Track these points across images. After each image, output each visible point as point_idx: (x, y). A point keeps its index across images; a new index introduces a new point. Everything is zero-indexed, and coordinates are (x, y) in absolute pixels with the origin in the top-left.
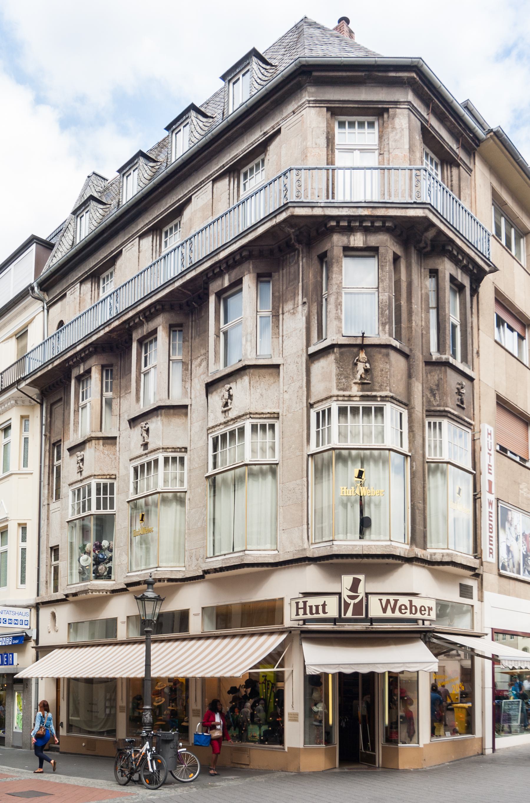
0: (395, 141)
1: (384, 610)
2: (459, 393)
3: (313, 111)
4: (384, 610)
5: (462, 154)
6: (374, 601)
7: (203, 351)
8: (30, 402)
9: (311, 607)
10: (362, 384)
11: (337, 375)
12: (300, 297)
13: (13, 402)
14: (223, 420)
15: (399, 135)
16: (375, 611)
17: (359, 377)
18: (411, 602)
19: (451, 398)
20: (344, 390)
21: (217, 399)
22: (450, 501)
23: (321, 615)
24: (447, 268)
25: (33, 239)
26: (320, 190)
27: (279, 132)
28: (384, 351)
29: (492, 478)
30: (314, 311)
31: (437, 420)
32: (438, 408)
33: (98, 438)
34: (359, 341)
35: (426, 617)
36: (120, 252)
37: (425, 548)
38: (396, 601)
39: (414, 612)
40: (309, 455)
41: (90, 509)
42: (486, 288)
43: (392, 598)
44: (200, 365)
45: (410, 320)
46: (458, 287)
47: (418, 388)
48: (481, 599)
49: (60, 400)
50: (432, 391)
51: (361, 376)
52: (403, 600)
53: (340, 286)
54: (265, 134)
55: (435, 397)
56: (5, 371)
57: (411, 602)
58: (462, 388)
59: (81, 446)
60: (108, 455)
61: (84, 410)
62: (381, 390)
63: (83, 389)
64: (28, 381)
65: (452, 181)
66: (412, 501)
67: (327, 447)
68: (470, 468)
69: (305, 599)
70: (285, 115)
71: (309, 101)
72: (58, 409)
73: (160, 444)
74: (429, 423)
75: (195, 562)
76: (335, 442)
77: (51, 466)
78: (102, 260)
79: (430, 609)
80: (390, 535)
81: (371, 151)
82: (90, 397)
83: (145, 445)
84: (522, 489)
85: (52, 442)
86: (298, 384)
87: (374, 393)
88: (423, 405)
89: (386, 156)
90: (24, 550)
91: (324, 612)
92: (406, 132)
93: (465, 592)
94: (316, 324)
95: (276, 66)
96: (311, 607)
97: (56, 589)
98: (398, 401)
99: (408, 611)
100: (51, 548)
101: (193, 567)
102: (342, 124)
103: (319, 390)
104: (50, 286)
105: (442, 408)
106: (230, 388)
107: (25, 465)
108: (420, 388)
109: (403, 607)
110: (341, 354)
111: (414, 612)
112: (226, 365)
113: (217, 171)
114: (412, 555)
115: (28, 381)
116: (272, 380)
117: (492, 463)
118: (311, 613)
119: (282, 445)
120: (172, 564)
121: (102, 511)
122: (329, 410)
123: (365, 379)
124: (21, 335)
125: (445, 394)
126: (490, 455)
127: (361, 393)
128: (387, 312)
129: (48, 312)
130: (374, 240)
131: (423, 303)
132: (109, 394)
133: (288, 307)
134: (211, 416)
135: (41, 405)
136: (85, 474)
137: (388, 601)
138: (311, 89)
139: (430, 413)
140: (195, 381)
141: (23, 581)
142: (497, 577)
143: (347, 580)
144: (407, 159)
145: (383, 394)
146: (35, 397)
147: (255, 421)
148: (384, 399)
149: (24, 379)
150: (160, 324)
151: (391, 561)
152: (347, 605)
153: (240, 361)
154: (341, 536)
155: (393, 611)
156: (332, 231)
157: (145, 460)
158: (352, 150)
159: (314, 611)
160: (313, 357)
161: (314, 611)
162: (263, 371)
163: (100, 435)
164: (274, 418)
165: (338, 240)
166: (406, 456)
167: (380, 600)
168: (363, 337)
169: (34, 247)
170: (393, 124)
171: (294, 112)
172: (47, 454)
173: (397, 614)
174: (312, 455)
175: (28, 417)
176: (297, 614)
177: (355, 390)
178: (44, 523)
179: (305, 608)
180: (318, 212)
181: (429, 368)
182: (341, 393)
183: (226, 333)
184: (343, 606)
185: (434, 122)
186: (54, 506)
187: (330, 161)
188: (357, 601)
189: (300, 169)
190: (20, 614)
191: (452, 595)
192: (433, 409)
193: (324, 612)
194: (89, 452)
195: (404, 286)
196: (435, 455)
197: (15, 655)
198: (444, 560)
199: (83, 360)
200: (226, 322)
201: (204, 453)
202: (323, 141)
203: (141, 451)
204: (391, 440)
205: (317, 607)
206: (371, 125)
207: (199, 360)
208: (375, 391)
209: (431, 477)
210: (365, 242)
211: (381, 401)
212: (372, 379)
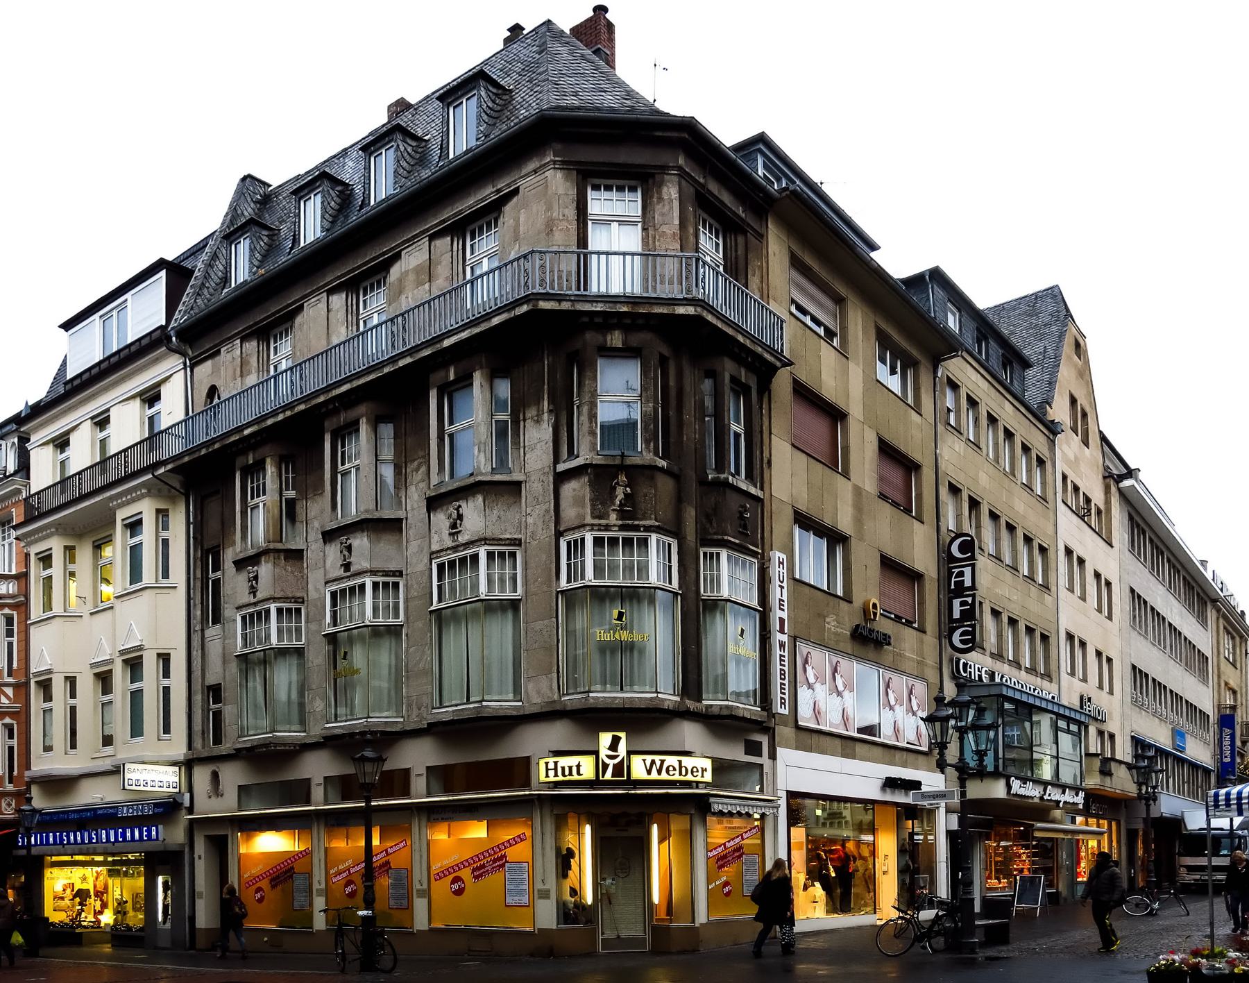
0: (663, 215)
1: (649, 772)
2: (742, 517)
3: (559, 174)
4: (649, 772)
5: (751, 220)
7: (421, 453)
9: (563, 768)
10: (622, 514)
11: (591, 500)
12: (546, 403)
14: (450, 544)
15: (667, 208)
18: (680, 762)
20: (600, 518)
21: (441, 520)
22: (733, 642)
23: (575, 777)
24: (728, 368)
25: (160, 264)
26: (569, 273)
27: (516, 192)
29: (784, 615)
30: (564, 421)
31: (714, 550)
33: (278, 551)
34: (618, 462)
35: (699, 779)
36: (301, 308)
37: (700, 700)
38: (662, 762)
40: (558, 592)
42: (782, 383)
43: (657, 758)
44: (417, 470)
45: (680, 434)
46: (740, 389)
47: (690, 514)
48: (773, 756)
49: (217, 492)
50: (708, 517)
52: (671, 760)
53: (594, 394)
54: (498, 191)
56: (133, 446)
57: (680, 762)
59: (254, 560)
60: (292, 573)
61: (255, 511)
62: (644, 519)
63: (252, 482)
64: (169, 467)
67: (580, 584)
68: (755, 603)
69: (556, 759)
70: (524, 172)
72: (213, 507)
73: (366, 565)
74: (705, 554)
75: (415, 712)
76: (590, 577)
77: (205, 578)
78: (273, 314)
79: (704, 770)
80: (660, 684)
81: (634, 223)
82: (264, 494)
83: (347, 567)
85: (205, 547)
86: (545, 507)
89: (651, 232)
90: (167, 690)
91: (579, 773)
92: (676, 204)
93: (753, 749)
94: (563, 441)
95: (511, 91)
96: (563, 768)
97: (218, 741)
100: (209, 688)
101: (414, 717)
102: (596, 188)
103: (570, 513)
104: (194, 337)
107: (166, 575)
108: (693, 513)
112: (452, 475)
113: (437, 225)
114: (683, 709)
115: (169, 467)
116: (511, 500)
117: (785, 598)
118: (564, 775)
119: (525, 577)
120: (385, 714)
122: (583, 540)
126: (782, 587)
129: (192, 371)
130: (637, 339)
132: (291, 494)
133: (532, 412)
134: (435, 538)
136: (260, 596)
137: (653, 762)
139: (706, 542)
140: (412, 489)
141: (167, 730)
142: (793, 730)
143: (605, 738)
144: (677, 238)
145: (647, 523)
146: (178, 487)
148: (648, 529)
149: (164, 463)
150: (362, 411)
151: (657, 715)
152: (605, 766)
153: (472, 475)
154: (599, 687)
155: (659, 772)
157: (346, 584)
158: (608, 223)
159: (567, 772)
160: (561, 478)
161: (567, 772)
163: (279, 546)
164: (514, 545)
166: (676, 594)
168: (623, 456)
169: (163, 273)
170: (660, 193)
171: (535, 171)
172: (199, 563)
173: (664, 776)
174: (562, 592)
176: (547, 776)
177: (613, 518)
178: (196, 654)
179: (556, 769)
180: (566, 306)
182: (596, 521)
183: (451, 436)
184: (600, 767)
185: (713, 187)
186: (213, 631)
187: (582, 241)
188: (616, 761)
189: (544, 252)
191: (736, 753)
193: (579, 773)
194: (265, 570)
195: (673, 393)
196: (712, 591)
197: (160, 827)
199: (254, 448)
200: (451, 423)
201: (425, 579)
202: (571, 212)
203: (341, 572)
204: (654, 578)
205: (570, 768)
206: (633, 189)
207: (416, 463)
209: (708, 619)
211: (645, 531)
212: (633, 506)
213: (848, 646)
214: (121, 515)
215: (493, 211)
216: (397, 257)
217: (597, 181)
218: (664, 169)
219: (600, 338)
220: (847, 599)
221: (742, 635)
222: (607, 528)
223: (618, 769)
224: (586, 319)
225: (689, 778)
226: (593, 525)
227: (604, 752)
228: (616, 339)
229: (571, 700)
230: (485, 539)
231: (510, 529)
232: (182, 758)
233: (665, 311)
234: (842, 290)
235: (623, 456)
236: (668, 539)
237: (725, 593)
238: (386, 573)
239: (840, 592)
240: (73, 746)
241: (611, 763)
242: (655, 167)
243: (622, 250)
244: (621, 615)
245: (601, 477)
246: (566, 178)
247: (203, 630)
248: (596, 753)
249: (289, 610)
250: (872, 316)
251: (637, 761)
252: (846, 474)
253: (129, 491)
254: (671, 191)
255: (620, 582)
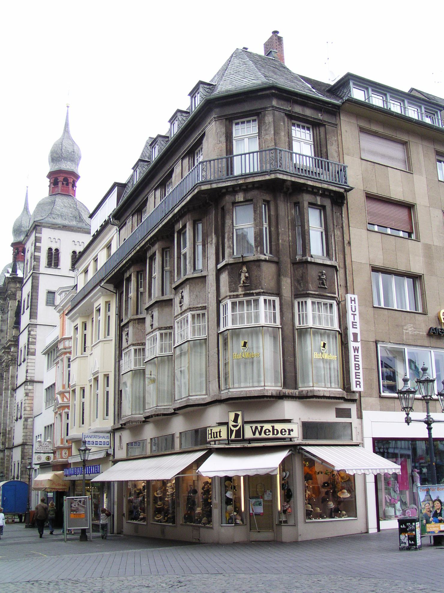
1: (254, 434)
2: (320, 279)
4: (254, 434)
6: (247, 428)
8: (106, 292)
9: (214, 433)
10: (245, 287)
13: (100, 293)
16: (248, 434)
17: (242, 282)
18: (273, 427)
19: (312, 284)
25: (116, 184)
28: (257, 263)
29: (358, 331)
31: (303, 300)
32: (302, 293)
34: (241, 260)
36: (147, 198)
37: (296, 388)
38: (262, 427)
39: (275, 433)
41: (225, 324)
43: (259, 426)
48: (360, 417)
50: (298, 282)
51: (243, 282)
55: (300, 285)
57: (273, 427)
58: (323, 275)
64: (105, 281)
65: (320, 136)
66: (283, 357)
71: (215, 118)
81: (255, 137)
84: (406, 330)
87: (251, 292)
88: (292, 292)
91: (220, 437)
93: (343, 413)
94: (219, 254)
96: (214, 433)
98: (270, 293)
99: (271, 433)
105: (305, 292)
106: (182, 292)
109: (267, 431)
110: (232, 269)
111: (275, 433)
121: (235, 327)
123: (246, 283)
124: (109, 247)
125: (307, 282)
126: (354, 315)
127: (243, 293)
128: (259, 239)
130: (249, 196)
131: (290, 225)
135: (116, 293)
137: (256, 428)
138: (217, 110)
139: (297, 295)
141: (107, 415)
142: (378, 399)
147: (193, 312)
148: (258, 294)
149: (103, 280)
150: (157, 248)
155: (260, 433)
156: (224, 194)
162: (197, 280)
164: (204, 309)
165: (228, 199)
167: (251, 427)
168: (242, 256)
169: (116, 189)
173: (263, 435)
175: (110, 301)
177: (240, 291)
181: (295, 266)
182: (232, 294)
188: (237, 428)
190: (103, 437)
192: (299, 293)
193: (220, 437)
198: (309, 395)
204: (262, 322)
208: (253, 290)
210: (244, 198)
213: (426, 342)
214: (96, 305)
215: (199, 142)
216: (172, 171)
217: (237, 121)
218: (265, 109)
219: (233, 198)
220: (425, 313)
221: (324, 346)
222: (237, 296)
223: (238, 433)
224: (224, 191)
225: (280, 435)
226: (230, 296)
227: (231, 423)
228: (240, 197)
229: (224, 395)
230: (190, 308)
231: (201, 301)
232: (110, 429)
233: (261, 179)
234: (405, 138)
235: (242, 256)
236: (272, 298)
237: (310, 324)
238: (166, 328)
239: (420, 311)
240: (83, 423)
241: (235, 429)
242: (261, 109)
243: (240, 153)
244: (245, 344)
245: (234, 269)
246: (221, 124)
247: (119, 361)
248: (227, 424)
249: (140, 349)
250: (432, 146)
251: (247, 428)
252: (417, 240)
253: (94, 295)
254: (269, 119)
255: (246, 325)
